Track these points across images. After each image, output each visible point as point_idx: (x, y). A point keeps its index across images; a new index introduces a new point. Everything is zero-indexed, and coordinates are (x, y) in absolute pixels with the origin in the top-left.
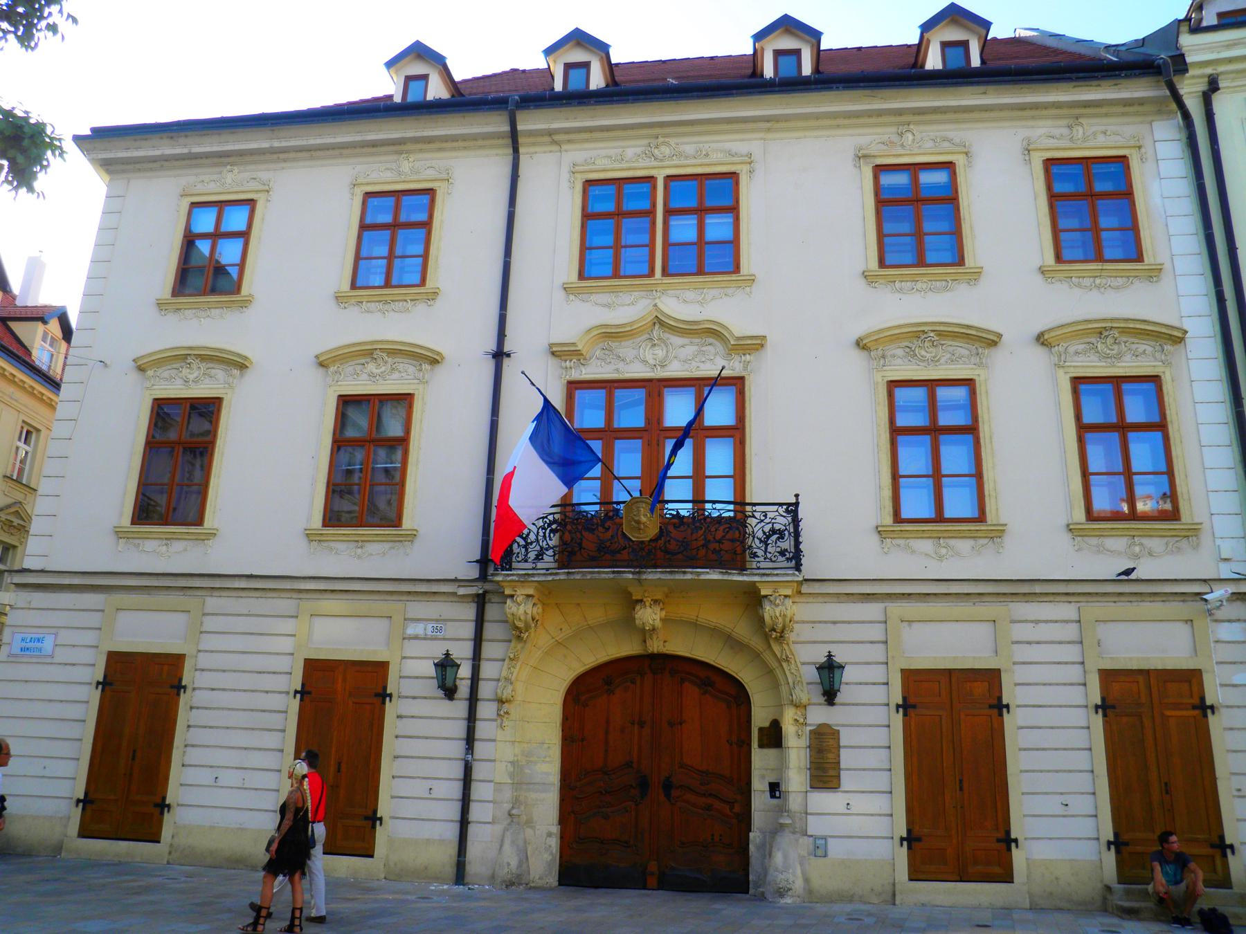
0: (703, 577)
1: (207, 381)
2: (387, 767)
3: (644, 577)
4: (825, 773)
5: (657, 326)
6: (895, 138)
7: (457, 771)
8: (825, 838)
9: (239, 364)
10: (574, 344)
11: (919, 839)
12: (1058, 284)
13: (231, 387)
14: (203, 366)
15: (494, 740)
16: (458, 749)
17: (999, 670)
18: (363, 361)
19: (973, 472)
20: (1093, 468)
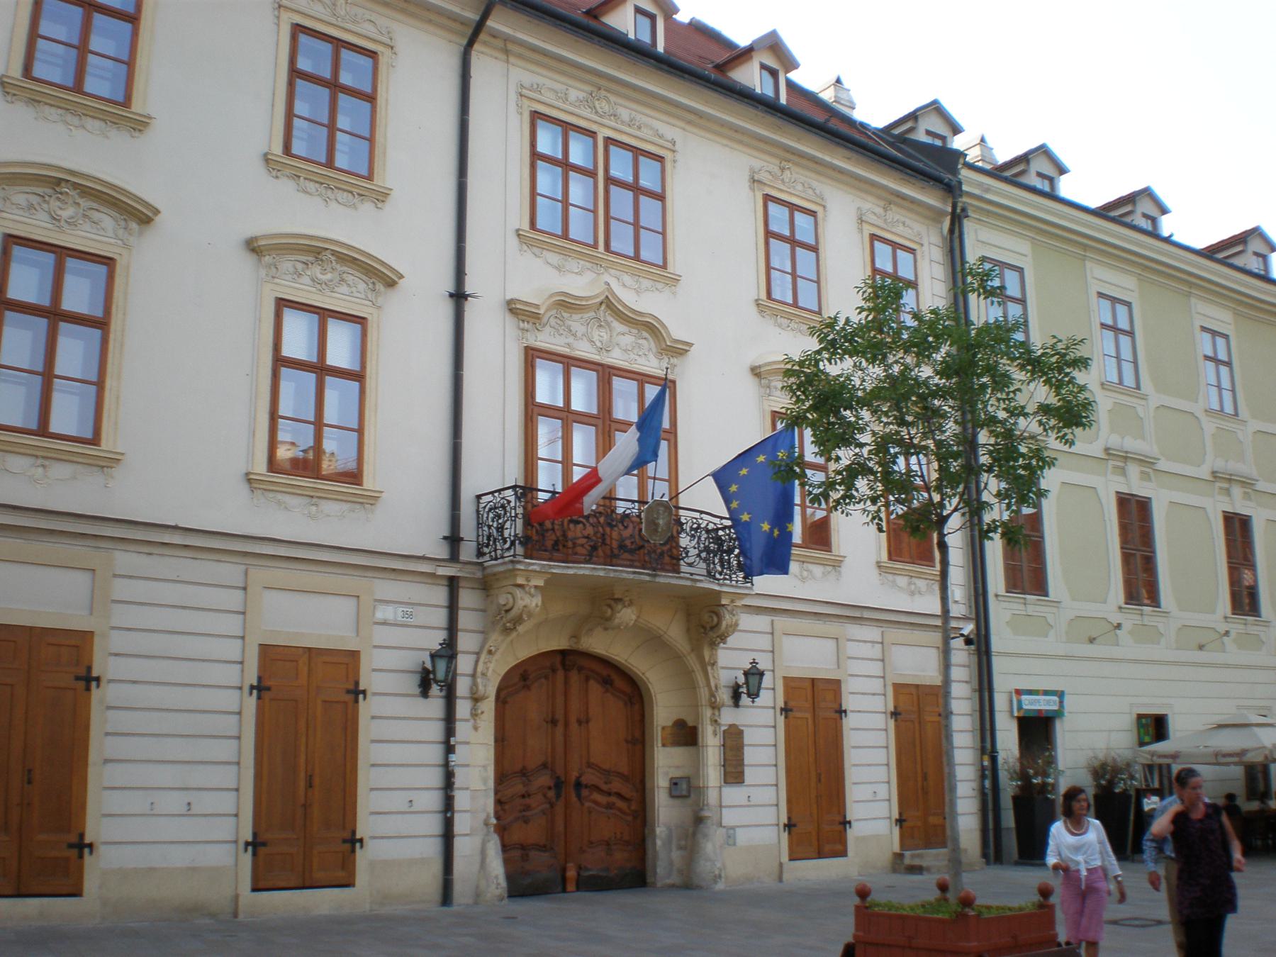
0: (699, 585)
1: (87, 226)
2: (366, 778)
3: (658, 579)
4: (734, 772)
5: (603, 307)
6: (776, 170)
7: (434, 778)
8: (733, 828)
9: (139, 215)
10: (537, 306)
11: (264, 844)
12: (285, 179)
13: (126, 246)
14: (84, 203)
15: (467, 743)
16: (434, 753)
17: (358, 652)
18: (304, 258)
19: (94, 378)
20: (282, 411)
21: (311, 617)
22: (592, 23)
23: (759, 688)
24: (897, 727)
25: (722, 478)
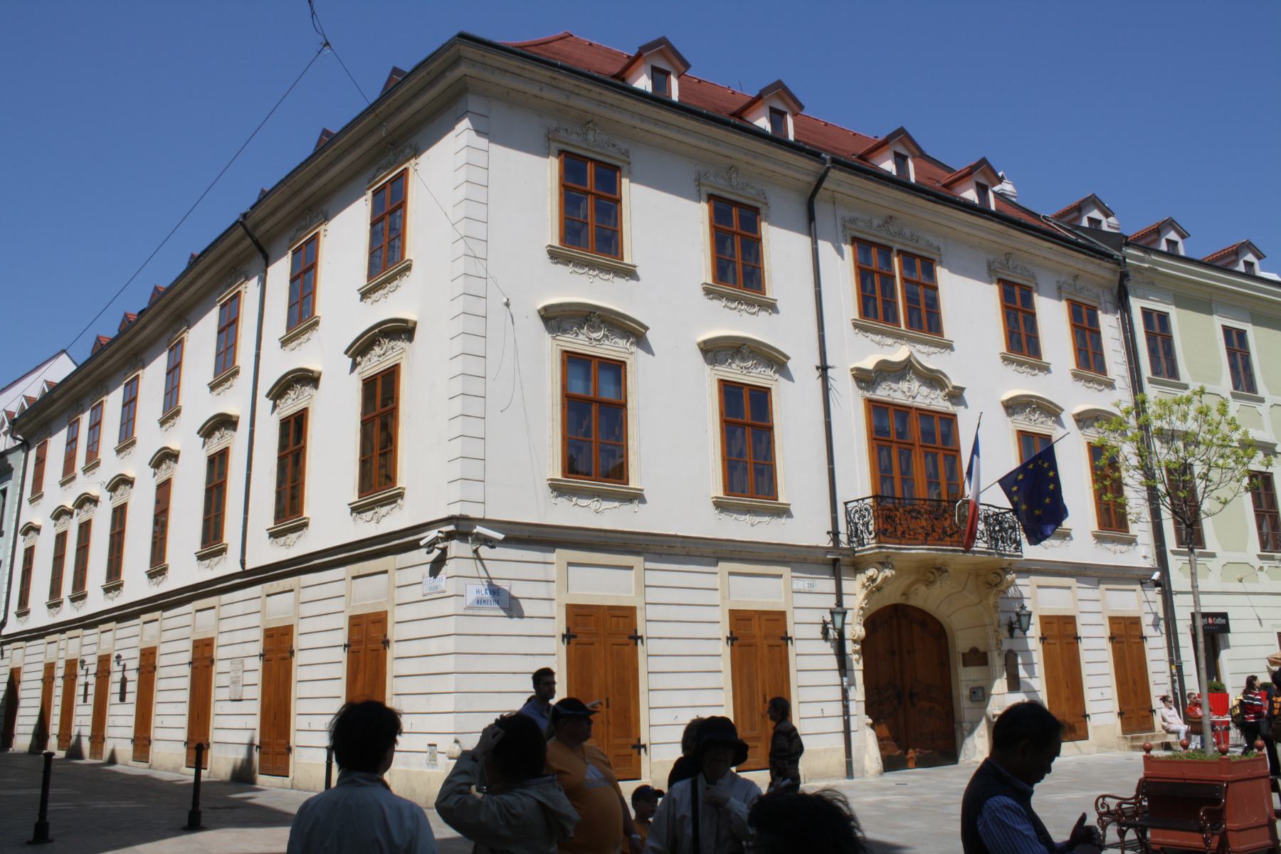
9: (634, 332)
21: (761, 591)
22: (866, 166)
23: (1029, 624)
24: (1113, 647)
25: (1006, 483)
